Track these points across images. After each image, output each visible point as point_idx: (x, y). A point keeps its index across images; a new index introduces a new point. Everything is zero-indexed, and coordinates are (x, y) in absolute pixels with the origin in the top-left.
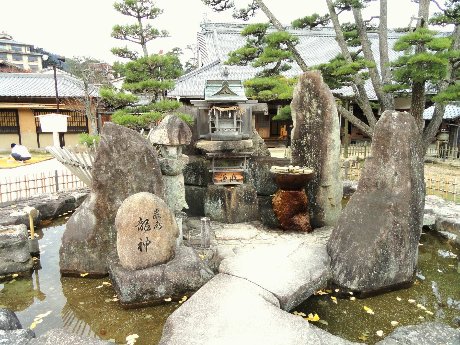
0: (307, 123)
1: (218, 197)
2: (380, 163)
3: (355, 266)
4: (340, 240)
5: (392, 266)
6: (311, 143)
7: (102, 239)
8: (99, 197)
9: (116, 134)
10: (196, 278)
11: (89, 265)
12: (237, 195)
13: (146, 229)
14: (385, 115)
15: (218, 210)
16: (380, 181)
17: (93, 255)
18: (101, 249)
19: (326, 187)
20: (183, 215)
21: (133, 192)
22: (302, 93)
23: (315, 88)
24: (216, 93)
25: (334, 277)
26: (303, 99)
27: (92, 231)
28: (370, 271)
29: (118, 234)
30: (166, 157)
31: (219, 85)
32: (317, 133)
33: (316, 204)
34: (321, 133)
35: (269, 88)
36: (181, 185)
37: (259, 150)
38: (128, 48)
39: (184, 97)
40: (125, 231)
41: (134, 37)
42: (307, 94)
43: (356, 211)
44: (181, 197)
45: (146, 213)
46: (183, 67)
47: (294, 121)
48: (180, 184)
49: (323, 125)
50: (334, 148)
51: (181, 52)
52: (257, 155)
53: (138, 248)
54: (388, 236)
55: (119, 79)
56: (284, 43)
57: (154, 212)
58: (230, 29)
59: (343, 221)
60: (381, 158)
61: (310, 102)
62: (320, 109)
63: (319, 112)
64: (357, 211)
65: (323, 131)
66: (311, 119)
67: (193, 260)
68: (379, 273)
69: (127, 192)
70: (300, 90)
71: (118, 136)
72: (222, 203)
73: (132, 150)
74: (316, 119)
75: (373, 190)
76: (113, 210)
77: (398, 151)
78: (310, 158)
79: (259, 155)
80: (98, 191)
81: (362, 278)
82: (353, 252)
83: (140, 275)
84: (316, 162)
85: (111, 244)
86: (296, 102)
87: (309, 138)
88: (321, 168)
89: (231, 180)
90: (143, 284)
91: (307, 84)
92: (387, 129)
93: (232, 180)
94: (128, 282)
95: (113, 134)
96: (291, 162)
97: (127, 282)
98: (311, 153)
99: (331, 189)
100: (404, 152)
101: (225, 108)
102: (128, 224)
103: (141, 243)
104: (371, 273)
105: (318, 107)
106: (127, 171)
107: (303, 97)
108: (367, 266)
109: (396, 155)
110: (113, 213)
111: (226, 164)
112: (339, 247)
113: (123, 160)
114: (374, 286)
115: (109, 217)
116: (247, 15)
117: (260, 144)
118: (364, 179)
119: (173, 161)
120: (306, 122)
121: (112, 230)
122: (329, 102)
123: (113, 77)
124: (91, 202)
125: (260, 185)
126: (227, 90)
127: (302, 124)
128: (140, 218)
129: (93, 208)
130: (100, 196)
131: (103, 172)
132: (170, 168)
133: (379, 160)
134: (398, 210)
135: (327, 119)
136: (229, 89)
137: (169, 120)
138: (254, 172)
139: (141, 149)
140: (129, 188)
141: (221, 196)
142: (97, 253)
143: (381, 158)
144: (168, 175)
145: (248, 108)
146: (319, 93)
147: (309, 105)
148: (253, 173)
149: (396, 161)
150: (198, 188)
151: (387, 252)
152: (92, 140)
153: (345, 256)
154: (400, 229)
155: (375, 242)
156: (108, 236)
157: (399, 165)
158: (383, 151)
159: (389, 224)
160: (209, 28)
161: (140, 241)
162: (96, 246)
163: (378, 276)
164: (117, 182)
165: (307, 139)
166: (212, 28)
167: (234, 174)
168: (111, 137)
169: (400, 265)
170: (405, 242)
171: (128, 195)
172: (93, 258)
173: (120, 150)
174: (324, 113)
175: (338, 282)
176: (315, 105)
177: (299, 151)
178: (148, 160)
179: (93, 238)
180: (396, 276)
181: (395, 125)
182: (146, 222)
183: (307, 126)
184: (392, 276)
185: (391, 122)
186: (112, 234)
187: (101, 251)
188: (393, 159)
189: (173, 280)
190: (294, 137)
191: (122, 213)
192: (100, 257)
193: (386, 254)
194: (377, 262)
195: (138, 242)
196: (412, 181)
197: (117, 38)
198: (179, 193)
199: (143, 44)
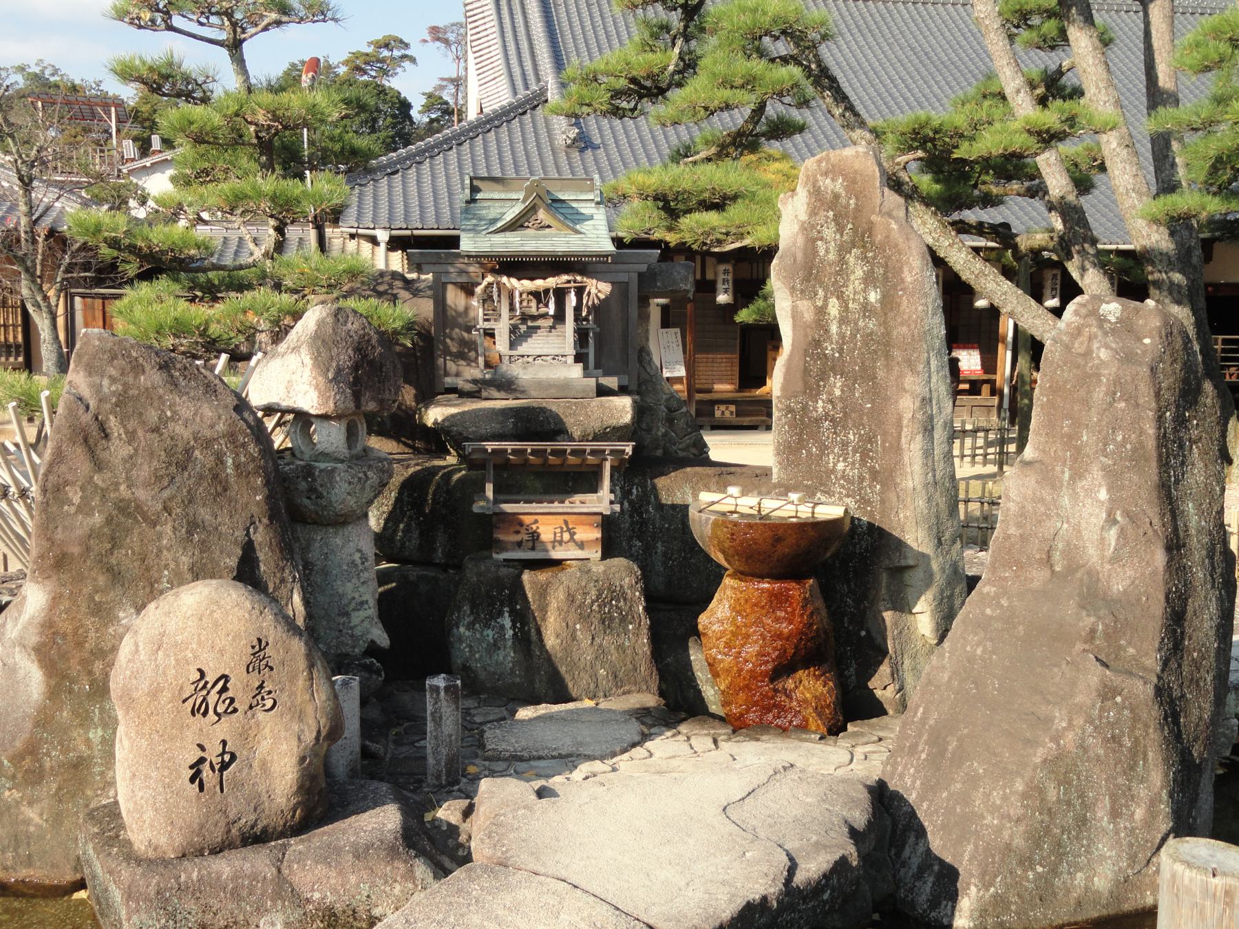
0: (830, 338)
1: (502, 605)
2: (1061, 481)
3: (970, 847)
4: (923, 756)
5: (1103, 848)
6: (844, 410)
7: (65, 751)
8: (55, 600)
9: (122, 374)
10: (398, 888)
11: (15, 850)
12: (571, 598)
13: (220, 709)
14: (1076, 313)
15: (502, 653)
16: (1060, 546)
17: (32, 814)
18: (59, 789)
20: (368, 668)
21: (178, 581)
22: (813, 227)
23: (858, 209)
25: (898, 888)
26: (815, 252)
27: (29, 725)
28: (1021, 863)
29: (121, 730)
30: (306, 457)
31: (515, 196)
32: (867, 375)
33: (863, 633)
34: (881, 374)
35: (718, 204)
36: (364, 559)
37: (665, 435)
38: (176, 59)
39: (408, 232)
40: (143, 716)
41: (203, 20)
42: (829, 232)
43: (979, 652)
44: (362, 603)
45: (222, 652)
46: (414, 113)
48: (357, 556)
49: (887, 344)
51: (407, 52)
52: (659, 453)
53: (192, 780)
54: (1083, 740)
55: (156, 158)
56: (777, 38)
57: (251, 651)
59: (938, 687)
60: (1064, 464)
61: (842, 261)
62: (875, 287)
63: (873, 296)
64: (984, 652)
65: (889, 368)
66: (843, 321)
67: (389, 826)
68: (1054, 872)
69: (158, 581)
70: (803, 217)
71: (130, 379)
72: (514, 627)
73: (179, 429)
74: (861, 323)
75: (1039, 576)
76: (106, 646)
77: (1119, 438)
78: (841, 466)
79: (666, 452)
80: (55, 578)
81: (992, 889)
82: (965, 799)
83: (195, 875)
84: (862, 479)
85: (97, 769)
86: (789, 262)
87: (838, 392)
88: (883, 501)
90: (206, 909)
91: (829, 197)
92: (1080, 361)
93: (561, 542)
94: (151, 901)
95: (113, 372)
96: (775, 478)
97: (147, 899)
98: (845, 445)
100: (1141, 443)
101: (532, 279)
102: (154, 694)
103: (202, 760)
104: (1025, 871)
105: (869, 280)
106: (160, 507)
107: (814, 241)
108: (1008, 847)
109: (1113, 452)
110: (106, 654)
111: (538, 485)
112: (918, 782)
113: (146, 467)
114: (1036, 919)
115: (90, 673)
117: (670, 410)
118: (1009, 537)
119: (333, 470)
120: (827, 331)
121: (101, 719)
122: (908, 263)
123: (130, 149)
124: (25, 617)
125: (664, 563)
127: (813, 346)
128: (199, 670)
129: (33, 639)
130: (61, 596)
131: (73, 509)
132: (320, 496)
133: (1058, 469)
134: (1120, 647)
135: (902, 324)
137: (321, 324)
138: (640, 514)
139: (212, 427)
140: (166, 567)
141: (511, 601)
142: (45, 803)
143: (1064, 464)
144: (315, 523)
145: (623, 277)
146: (870, 228)
147: (838, 273)
148: (636, 518)
150: (430, 573)
151: (1082, 796)
152: (38, 393)
153: (936, 811)
154: (1126, 712)
155: (1038, 760)
156: (88, 742)
157: (1122, 488)
158: (1070, 437)
159: (1085, 695)
161: (200, 754)
162: (42, 777)
163: (1049, 884)
164: (121, 547)
165: (830, 393)
167: (566, 522)
168: (106, 382)
169: (1131, 845)
170: (1145, 759)
171: (161, 592)
172: (28, 822)
173: (134, 431)
175: (913, 905)
176: (859, 273)
177: (801, 440)
178: (237, 466)
179: (32, 749)
180: (1117, 883)
181: (1107, 347)
182: (221, 684)
183: (829, 348)
184: (1102, 881)
185: (1096, 337)
186: (100, 732)
187: (58, 797)
189: (317, 895)
190: (784, 388)
191: (137, 651)
192: (57, 819)
193: (1077, 803)
194: (1047, 831)
195: (196, 754)
197: (140, 27)
198: (356, 588)
199: (235, 47)
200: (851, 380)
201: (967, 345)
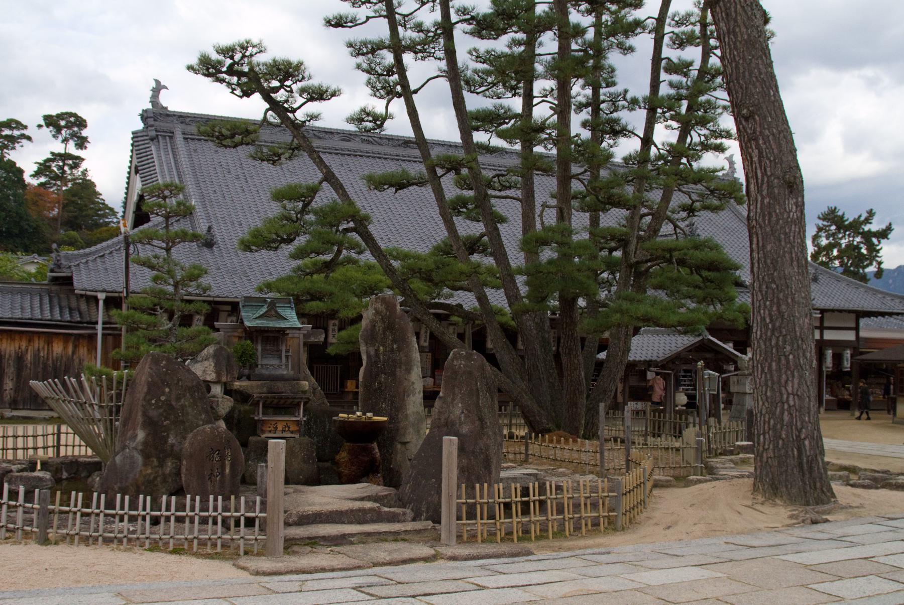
8: (147, 435)
19: (404, 443)
24: (258, 315)
34: (398, 373)
47: (364, 357)
89: (283, 431)
116: (280, 159)
127: (372, 363)
129: (140, 447)
136: (276, 312)
160: (162, 125)
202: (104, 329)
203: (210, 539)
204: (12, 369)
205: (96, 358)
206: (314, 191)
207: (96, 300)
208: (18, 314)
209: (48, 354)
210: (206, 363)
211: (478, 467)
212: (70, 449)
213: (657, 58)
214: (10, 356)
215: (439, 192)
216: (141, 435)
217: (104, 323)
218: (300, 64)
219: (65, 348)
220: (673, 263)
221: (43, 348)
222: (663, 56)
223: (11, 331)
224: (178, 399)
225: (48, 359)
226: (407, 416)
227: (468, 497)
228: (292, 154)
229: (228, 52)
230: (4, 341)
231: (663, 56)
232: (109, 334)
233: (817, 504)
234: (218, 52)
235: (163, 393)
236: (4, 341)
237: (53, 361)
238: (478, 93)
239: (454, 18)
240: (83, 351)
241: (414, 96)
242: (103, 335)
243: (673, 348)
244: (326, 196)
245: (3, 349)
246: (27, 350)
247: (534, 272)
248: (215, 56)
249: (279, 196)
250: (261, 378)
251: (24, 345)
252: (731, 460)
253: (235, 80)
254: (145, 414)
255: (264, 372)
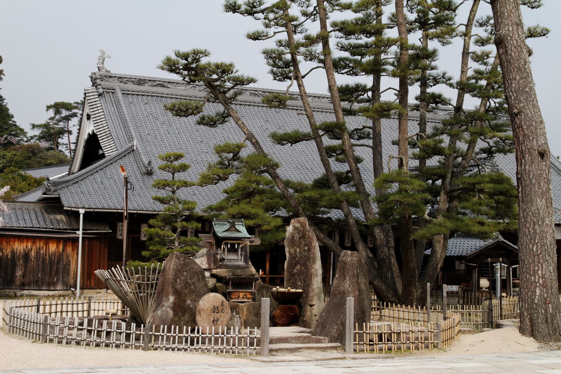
8: (176, 299)
19: (312, 306)
34: (308, 264)
42: (297, 235)
47: (287, 254)
50: (317, 276)
58: (146, 88)
89: (243, 298)
98: (300, 279)
99: (315, 307)
126: (233, 229)
127: (293, 257)
129: (171, 306)
146: (305, 234)
149: (350, 279)
166: (113, 84)
174: (309, 250)
188: (348, 277)
190: (287, 267)
196: (359, 291)
200: (302, 265)
201: (504, 292)
202: (83, 234)
203: (231, 349)
204: (22, 262)
205: (77, 254)
206: (239, 147)
207: (78, 213)
208: (22, 224)
209: (46, 251)
210: (203, 259)
211: (362, 317)
212: (96, 312)
213: (465, 53)
214: (20, 253)
215: (319, 144)
216: (172, 299)
217: (83, 230)
218: (231, 65)
219: (58, 247)
220: (475, 192)
221: (43, 247)
222: (470, 51)
223: (21, 236)
224: (191, 279)
225: (46, 255)
226: (313, 291)
227: (359, 330)
228: (223, 120)
229: (185, 56)
230: (16, 243)
231: (470, 51)
232: (86, 238)
233: (556, 341)
234: (176, 55)
235: (183, 276)
236: (16, 243)
237: (49, 257)
238: (342, 74)
239: (329, 28)
240: (69, 250)
241: (303, 80)
242: (83, 238)
243: (478, 248)
244: (247, 151)
245: (15, 248)
246: (32, 249)
247: (381, 199)
248: (174, 57)
249: (220, 150)
250: (227, 267)
251: (30, 245)
252: (513, 322)
253: (186, 72)
254: (173, 287)
255: (229, 263)
